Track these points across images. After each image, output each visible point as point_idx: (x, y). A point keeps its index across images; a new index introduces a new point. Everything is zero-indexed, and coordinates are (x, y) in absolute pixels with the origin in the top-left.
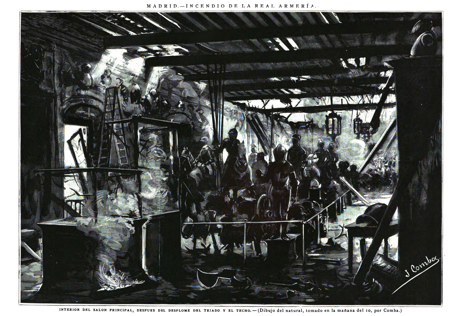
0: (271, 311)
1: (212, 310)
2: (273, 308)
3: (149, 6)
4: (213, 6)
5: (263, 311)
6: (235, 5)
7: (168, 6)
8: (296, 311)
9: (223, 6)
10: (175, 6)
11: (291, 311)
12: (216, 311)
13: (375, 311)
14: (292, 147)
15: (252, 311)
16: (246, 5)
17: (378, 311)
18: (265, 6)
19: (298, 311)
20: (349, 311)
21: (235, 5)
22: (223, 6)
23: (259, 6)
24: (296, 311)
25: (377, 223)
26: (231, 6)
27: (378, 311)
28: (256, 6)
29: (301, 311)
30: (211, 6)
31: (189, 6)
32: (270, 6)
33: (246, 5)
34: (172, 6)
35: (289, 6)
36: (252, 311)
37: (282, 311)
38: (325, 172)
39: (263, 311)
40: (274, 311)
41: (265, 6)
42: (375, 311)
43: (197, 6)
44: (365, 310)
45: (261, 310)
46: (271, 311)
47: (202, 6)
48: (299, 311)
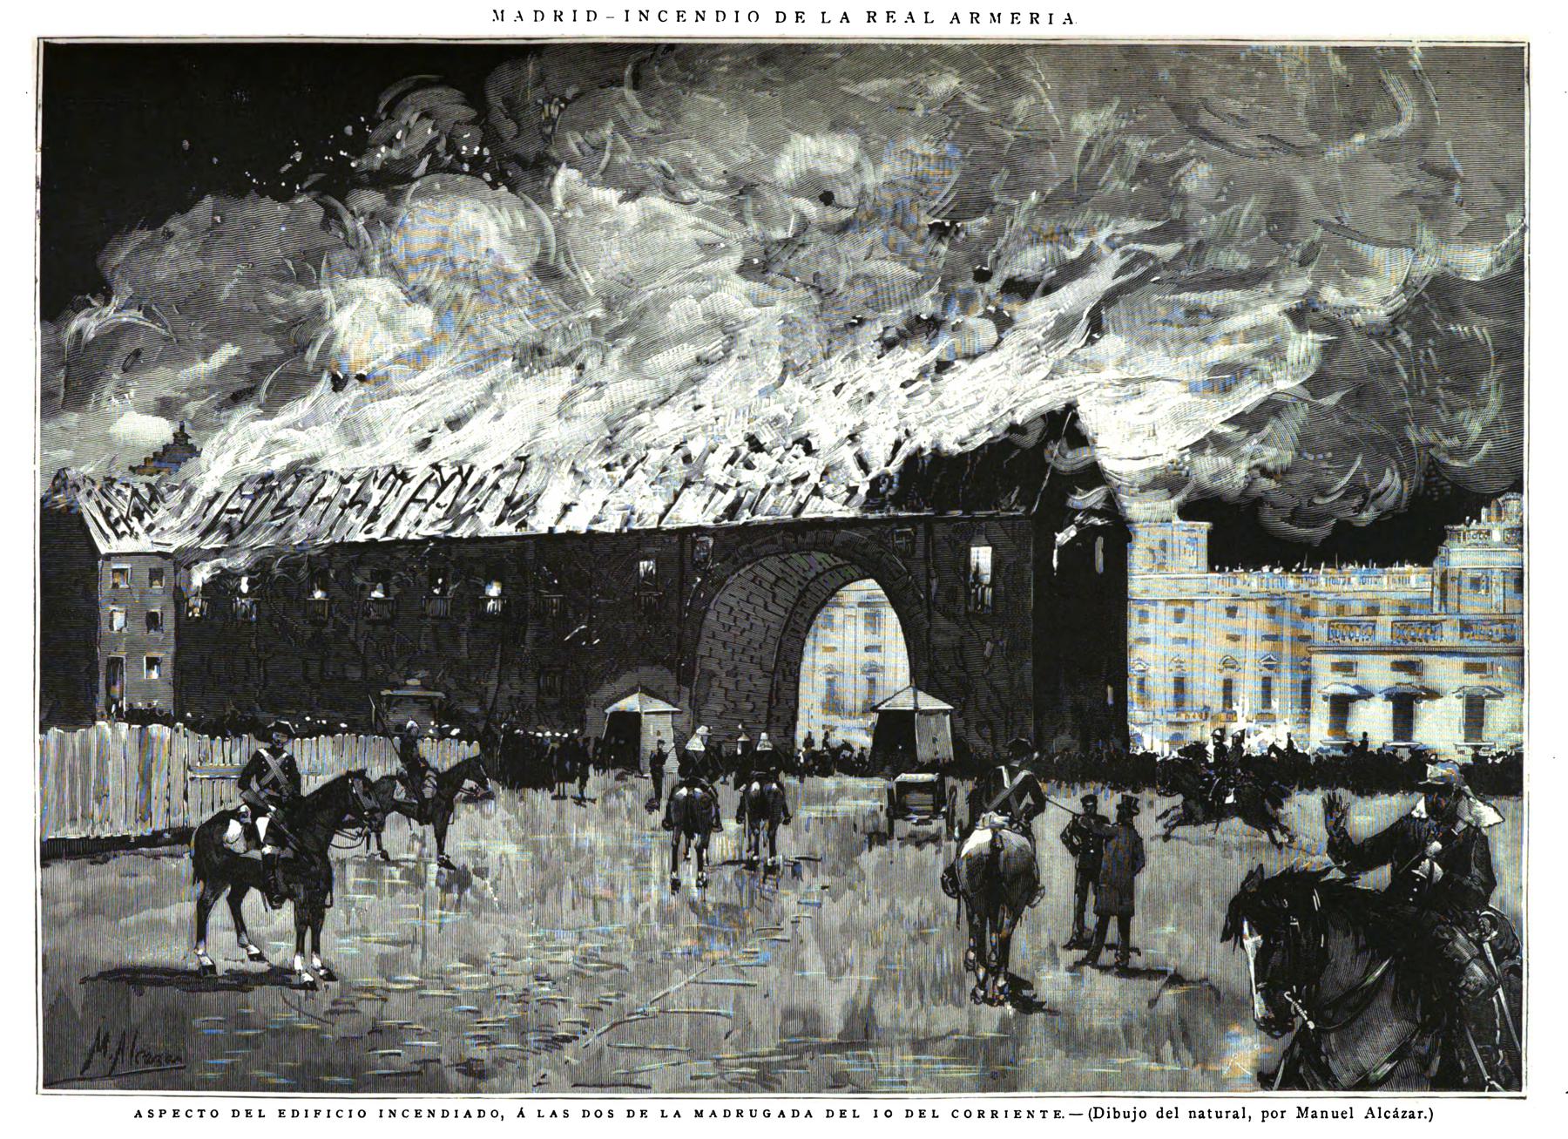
0: (1132, 1115)
1: (461, 1114)
2: (1142, 1105)
3: (499, 15)
4: (720, 15)
5: (1106, 1114)
6: (799, 16)
7: (568, 16)
8: (1224, 1115)
9: (753, 16)
10: (592, 15)
11: (1206, 1114)
12: (1099, 1113)
13: (1265, 1114)
14: (1224, 499)
15: (1067, 1116)
16: (834, 15)
17: (1274, 1115)
18: (901, 16)
19: (1230, 1115)
20: (1319, 1115)
21: (799, 16)
22: (753, 16)
23: (881, 17)
24: (1224, 1115)
25: (1026, 777)
26: (539, 15)
27: (1274, 1115)
28: (871, 17)
29: (1240, 1115)
30: (710, 16)
31: (634, 16)
32: (919, 17)
33: (834, 15)
34: (582, 16)
35: (985, 18)
36: (1067, 1116)
37: (1174, 1115)
38: (530, 594)
39: (1106, 1114)
40: (1143, 1115)
41: (1059, 18)
42: (1265, 1114)
43: (663, 16)
44: (1183, 1113)
45: (1096, 1113)
46: (1132, 1115)
47: (680, 15)
48: (1236, 1116)
